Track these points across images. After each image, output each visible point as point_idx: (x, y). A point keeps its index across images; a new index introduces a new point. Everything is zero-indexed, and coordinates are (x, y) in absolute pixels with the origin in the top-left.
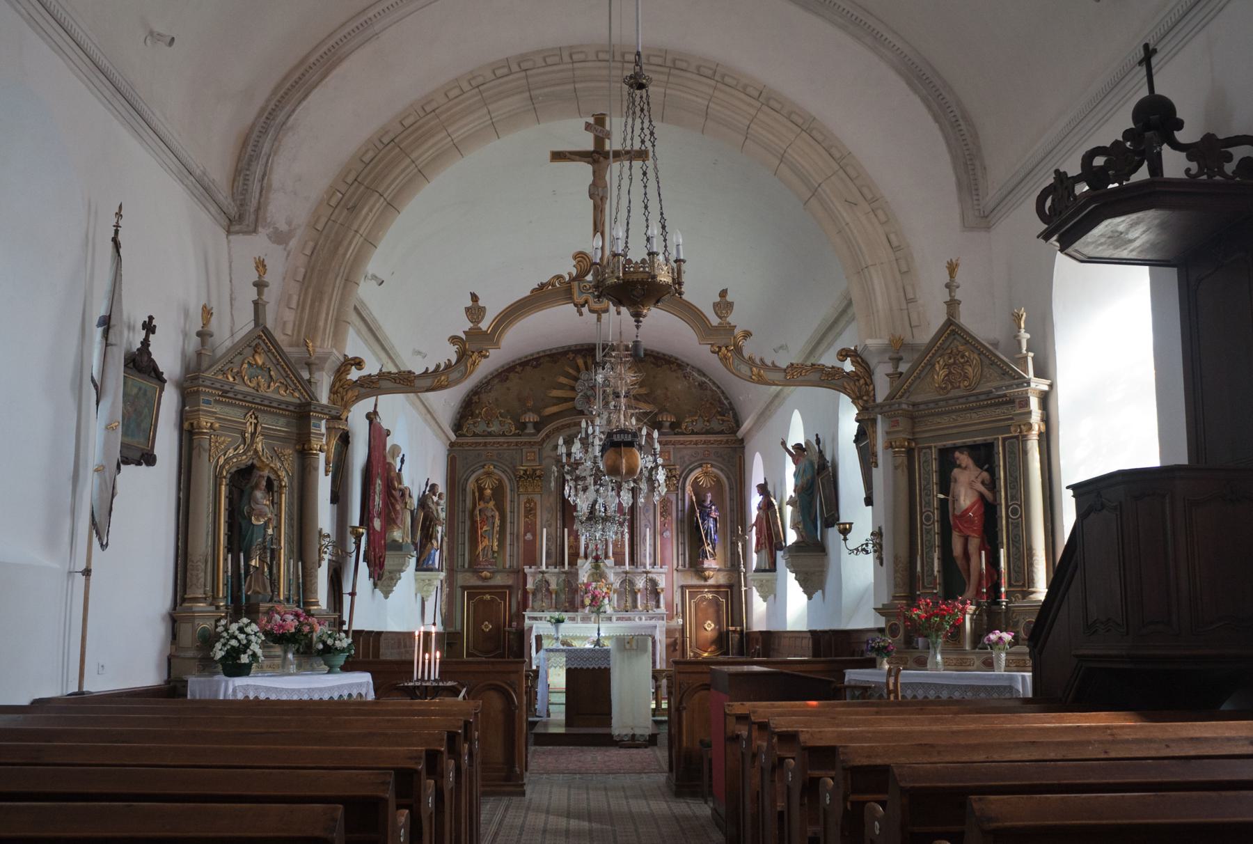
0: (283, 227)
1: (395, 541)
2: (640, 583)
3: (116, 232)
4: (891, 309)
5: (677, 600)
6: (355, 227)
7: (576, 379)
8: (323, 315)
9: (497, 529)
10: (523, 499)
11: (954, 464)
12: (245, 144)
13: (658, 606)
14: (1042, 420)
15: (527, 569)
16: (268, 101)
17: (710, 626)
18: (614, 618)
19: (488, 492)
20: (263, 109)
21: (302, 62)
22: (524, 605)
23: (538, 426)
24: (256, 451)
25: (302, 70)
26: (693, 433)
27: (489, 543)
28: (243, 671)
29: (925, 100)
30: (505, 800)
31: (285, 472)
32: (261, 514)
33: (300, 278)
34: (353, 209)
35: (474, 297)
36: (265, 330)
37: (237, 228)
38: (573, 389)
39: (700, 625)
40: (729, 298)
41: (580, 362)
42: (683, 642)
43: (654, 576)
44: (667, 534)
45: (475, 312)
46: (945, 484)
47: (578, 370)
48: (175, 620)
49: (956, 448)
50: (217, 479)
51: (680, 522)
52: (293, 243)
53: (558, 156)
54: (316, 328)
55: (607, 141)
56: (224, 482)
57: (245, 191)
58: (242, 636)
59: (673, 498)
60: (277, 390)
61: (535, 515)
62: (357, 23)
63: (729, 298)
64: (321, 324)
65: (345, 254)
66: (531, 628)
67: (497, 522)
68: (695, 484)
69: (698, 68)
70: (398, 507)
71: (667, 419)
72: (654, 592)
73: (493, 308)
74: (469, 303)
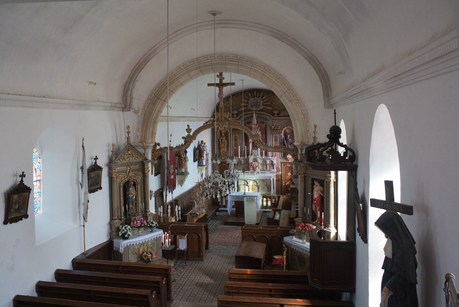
0: (136, 109)
1: (182, 172)
4: (302, 133)
5: (280, 167)
6: (155, 109)
7: (249, 100)
9: (226, 145)
12: (125, 87)
13: (274, 169)
14: (335, 178)
16: (130, 74)
17: (289, 174)
19: (223, 134)
20: (129, 76)
21: (139, 62)
23: (237, 115)
25: (139, 65)
26: (284, 116)
27: (224, 149)
28: (127, 238)
30: (198, 262)
31: (139, 179)
32: (131, 194)
33: (141, 124)
34: (154, 104)
35: (188, 126)
36: (131, 145)
37: (125, 110)
38: (248, 103)
39: (286, 174)
41: (250, 95)
42: (281, 179)
45: (189, 130)
47: (249, 97)
50: (120, 186)
52: (139, 114)
53: (209, 85)
54: (146, 137)
57: (126, 100)
58: (125, 230)
59: (278, 136)
60: (135, 159)
62: (152, 50)
64: (147, 136)
67: (226, 143)
71: (276, 112)
72: (272, 164)
74: (187, 128)
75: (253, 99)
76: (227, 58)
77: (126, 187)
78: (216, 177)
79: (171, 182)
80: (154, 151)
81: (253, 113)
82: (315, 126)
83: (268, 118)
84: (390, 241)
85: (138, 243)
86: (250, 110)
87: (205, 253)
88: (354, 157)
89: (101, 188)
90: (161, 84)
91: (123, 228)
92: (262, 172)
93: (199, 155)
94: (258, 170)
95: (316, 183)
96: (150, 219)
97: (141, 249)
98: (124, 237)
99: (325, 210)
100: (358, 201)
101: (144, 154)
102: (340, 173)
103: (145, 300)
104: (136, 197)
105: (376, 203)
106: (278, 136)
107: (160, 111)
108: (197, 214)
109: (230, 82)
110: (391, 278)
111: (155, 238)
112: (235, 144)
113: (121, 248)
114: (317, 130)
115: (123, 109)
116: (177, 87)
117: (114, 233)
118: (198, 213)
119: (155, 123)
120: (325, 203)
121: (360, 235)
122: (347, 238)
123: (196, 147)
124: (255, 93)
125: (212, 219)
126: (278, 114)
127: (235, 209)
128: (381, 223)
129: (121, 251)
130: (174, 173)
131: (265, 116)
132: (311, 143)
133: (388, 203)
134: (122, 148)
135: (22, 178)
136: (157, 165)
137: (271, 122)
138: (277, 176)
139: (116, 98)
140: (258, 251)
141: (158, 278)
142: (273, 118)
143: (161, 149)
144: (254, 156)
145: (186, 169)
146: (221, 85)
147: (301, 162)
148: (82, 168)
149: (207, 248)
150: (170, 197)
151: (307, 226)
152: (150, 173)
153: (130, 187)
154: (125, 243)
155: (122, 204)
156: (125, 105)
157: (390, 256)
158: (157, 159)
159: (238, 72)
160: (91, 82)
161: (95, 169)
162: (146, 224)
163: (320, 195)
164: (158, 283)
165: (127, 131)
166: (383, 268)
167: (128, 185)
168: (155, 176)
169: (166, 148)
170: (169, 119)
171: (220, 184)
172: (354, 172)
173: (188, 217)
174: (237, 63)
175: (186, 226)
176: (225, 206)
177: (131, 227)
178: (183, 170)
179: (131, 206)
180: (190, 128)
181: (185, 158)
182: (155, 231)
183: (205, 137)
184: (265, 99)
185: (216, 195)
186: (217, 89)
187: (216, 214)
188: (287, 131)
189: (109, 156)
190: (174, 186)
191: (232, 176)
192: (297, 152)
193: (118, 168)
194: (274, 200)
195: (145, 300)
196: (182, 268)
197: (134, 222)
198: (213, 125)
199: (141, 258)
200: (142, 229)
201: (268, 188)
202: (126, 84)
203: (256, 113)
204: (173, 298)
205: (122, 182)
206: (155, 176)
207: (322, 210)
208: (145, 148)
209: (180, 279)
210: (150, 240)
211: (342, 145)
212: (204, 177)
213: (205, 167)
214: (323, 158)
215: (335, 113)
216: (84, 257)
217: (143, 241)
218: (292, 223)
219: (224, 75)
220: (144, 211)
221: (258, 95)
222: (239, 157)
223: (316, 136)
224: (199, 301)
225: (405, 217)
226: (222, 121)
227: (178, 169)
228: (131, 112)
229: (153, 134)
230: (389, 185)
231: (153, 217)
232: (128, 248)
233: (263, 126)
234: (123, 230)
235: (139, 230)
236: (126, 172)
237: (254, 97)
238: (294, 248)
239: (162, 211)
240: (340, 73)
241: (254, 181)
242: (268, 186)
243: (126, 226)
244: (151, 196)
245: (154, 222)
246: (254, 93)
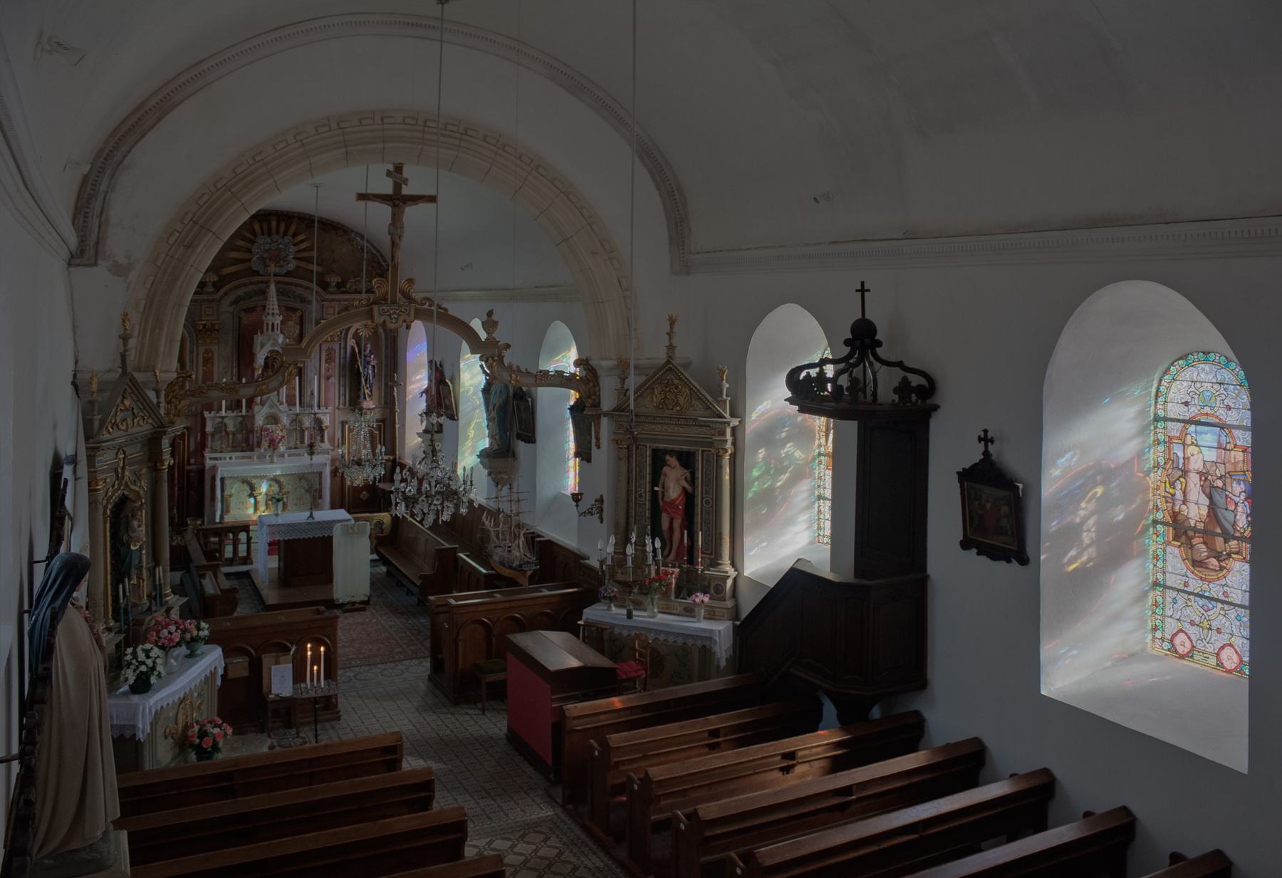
2: (307, 423)
7: (252, 242)
10: (202, 350)
11: (664, 463)
13: (322, 441)
15: (206, 414)
22: (202, 446)
33: (141, 309)
34: (190, 246)
37: (77, 261)
38: (249, 251)
40: (495, 318)
44: (332, 380)
46: (656, 478)
49: (665, 452)
51: (342, 367)
59: (336, 347)
63: (495, 318)
66: (214, 468)
69: (485, 137)
71: (334, 280)
75: (268, 240)
81: (267, 283)
86: (257, 273)
92: (293, 451)
97: (181, 717)
112: (205, 373)
124: (274, 224)
126: (339, 286)
131: (300, 291)
135: (986, 446)
144: (271, 407)
163: (684, 489)
174: (457, 142)
184: (302, 241)
188: (362, 333)
199: (183, 743)
203: (277, 283)
205: (108, 502)
219: (407, 172)
221: (265, 227)
226: (394, 302)
237: (270, 235)
241: (276, 480)
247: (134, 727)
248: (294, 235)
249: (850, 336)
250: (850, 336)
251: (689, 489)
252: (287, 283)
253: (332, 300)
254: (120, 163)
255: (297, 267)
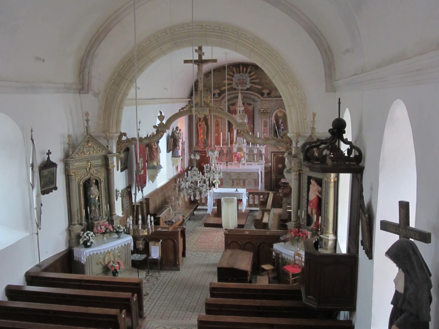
1: (154, 166)
2: (256, 152)
3: (32, 136)
5: (269, 157)
7: (233, 76)
8: (112, 121)
9: (205, 131)
12: (81, 63)
18: (246, 164)
23: (220, 95)
24: (91, 174)
29: (315, 41)
30: (173, 272)
31: (102, 176)
32: (93, 195)
36: (91, 135)
37: (82, 92)
38: (232, 80)
41: (234, 70)
43: (261, 149)
47: (234, 73)
48: (69, 231)
50: (79, 185)
52: (100, 97)
53: (186, 62)
55: (203, 56)
56: (81, 186)
58: (88, 237)
59: (268, 120)
60: (97, 152)
61: (219, 126)
64: (111, 124)
65: (117, 100)
68: (276, 115)
70: (155, 154)
71: (266, 91)
73: (167, 116)
74: (159, 114)
76: (207, 27)
77: (87, 185)
78: (195, 175)
79: (140, 179)
80: (120, 142)
81: (238, 93)
82: (314, 115)
83: (256, 99)
84: (403, 275)
85: (102, 252)
86: (235, 89)
87: (182, 261)
88: (359, 158)
89: (56, 188)
90: (127, 60)
91: (85, 235)
93: (173, 145)
94: (243, 161)
95: (313, 182)
96: (117, 223)
97: (107, 259)
98: (86, 245)
99: (323, 214)
100: (363, 211)
101: (108, 147)
102: (342, 175)
103: (113, 321)
104: (99, 198)
105: (386, 226)
106: (268, 120)
107: (126, 94)
108: (172, 222)
109: (210, 58)
110: (400, 316)
111: (123, 245)
113: (82, 258)
114: (315, 120)
115: (80, 90)
116: (145, 65)
117: (74, 241)
118: (174, 221)
119: (120, 108)
120: (323, 207)
121: (364, 249)
122: (349, 249)
123: (170, 134)
124: (241, 68)
125: (190, 219)
126: (269, 94)
127: (216, 207)
128: (395, 254)
129: (82, 262)
130: (144, 168)
132: (310, 134)
133: (402, 227)
134: (80, 139)
136: (123, 159)
137: (261, 104)
138: (266, 168)
139: (70, 76)
140: (244, 261)
141: (127, 295)
142: (262, 98)
143: (128, 140)
144: (239, 144)
145: (159, 161)
146: (200, 62)
147: (295, 157)
148: (32, 166)
149: (184, 255)
150: (138, 197)
151: (301, 232)
152: (115, 169)
153: (91, 186)
154: (87, 252)
155: (83, 206)
156: (82, 86)
157: (401, 291)
158: (124, 152)
159: (221, 46)
160: (38, 59)
161: (48, 166)
162: (112, 230)
164: (128, 300)
165: (85, 118)
166: (392, 303)
167: (89, 183)
168: (121, 172)
169: (134, 139)
170: (137, 102)
171: (200, 183)
172: (359, 175)
173: (161, 219)
175: (160, 231)
176: (205, 204)
177: (94, 233)
178: (155, 163)
179: (93, 208)
180: (163, 114)
181: (158, 150)
182: (123, 238)
183: (182, 124)
184: (253, 75)
185: (195, 196)
186: (196, 66)
187: (194, 213)
188: (280, 115)
189: (64, 149)
190: (145, 183)
191: (214, 172)
192: (291, 145)
193: (76, 164)
194: (262, 196)
195: (113, 321)
196: (155, 279)
197: (97, 227)
198: (191, 111)
199: (106, 269)
200: (108, 235)
201: (255, 183)
202: (82, 59)
203: (241, 93)
204: (145, 315)
206: (121, 172)
207: (319, 214)
208: (107, 139)
209: (154, 293)
210: (116, 247)
211: (346, 142)
212: (179, 169)
213: (181, 158)
214: (323, 159)
215: (339, 103)
216: (39, 269)
217: (107, 250)
218: (283, 223)
219: (204, 49)
220: (109, 214)
221: (245, 69)
222: (221, 146)
223: (315, 127)
224: (176, 319)
225: (420, 245)
227: (149, 162)
228: (90, 96)
229: (118, 122)
230: (404, 207)
231: (120, 221)
232: (91, 258)
233: (251, 108)
234: (85, 237)
235: (103, 236)
236: (86, 169)
238: (286, 257)
239: (131, 222)
240: (347, 51)
242: (255, 180)
243: (88, 232)
244: (117, 196)
245: (122, 227)
246: (239, 67)
247: (81, 258)
248: (250, 73)
249: (332, 128)
250: (332, 128)
251: (319, 195)
252: (247, 93)
253: (266, 101)
254: (94, 54)
255: (251, 86)
